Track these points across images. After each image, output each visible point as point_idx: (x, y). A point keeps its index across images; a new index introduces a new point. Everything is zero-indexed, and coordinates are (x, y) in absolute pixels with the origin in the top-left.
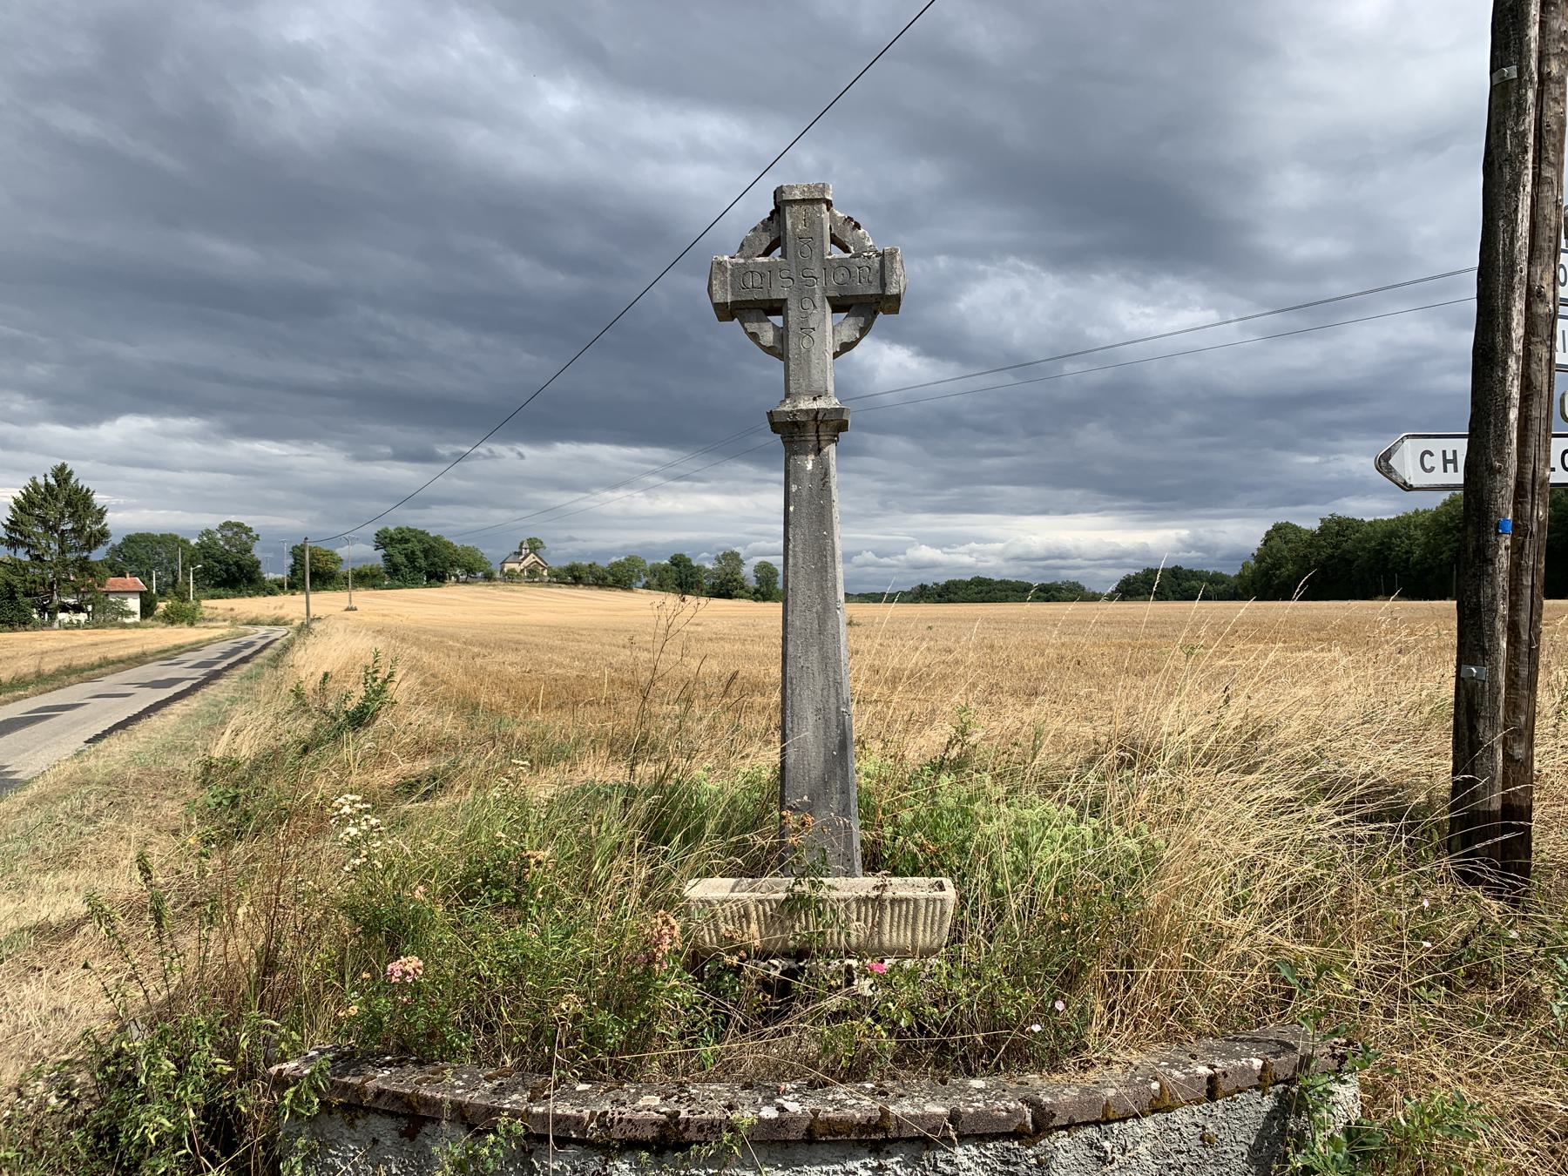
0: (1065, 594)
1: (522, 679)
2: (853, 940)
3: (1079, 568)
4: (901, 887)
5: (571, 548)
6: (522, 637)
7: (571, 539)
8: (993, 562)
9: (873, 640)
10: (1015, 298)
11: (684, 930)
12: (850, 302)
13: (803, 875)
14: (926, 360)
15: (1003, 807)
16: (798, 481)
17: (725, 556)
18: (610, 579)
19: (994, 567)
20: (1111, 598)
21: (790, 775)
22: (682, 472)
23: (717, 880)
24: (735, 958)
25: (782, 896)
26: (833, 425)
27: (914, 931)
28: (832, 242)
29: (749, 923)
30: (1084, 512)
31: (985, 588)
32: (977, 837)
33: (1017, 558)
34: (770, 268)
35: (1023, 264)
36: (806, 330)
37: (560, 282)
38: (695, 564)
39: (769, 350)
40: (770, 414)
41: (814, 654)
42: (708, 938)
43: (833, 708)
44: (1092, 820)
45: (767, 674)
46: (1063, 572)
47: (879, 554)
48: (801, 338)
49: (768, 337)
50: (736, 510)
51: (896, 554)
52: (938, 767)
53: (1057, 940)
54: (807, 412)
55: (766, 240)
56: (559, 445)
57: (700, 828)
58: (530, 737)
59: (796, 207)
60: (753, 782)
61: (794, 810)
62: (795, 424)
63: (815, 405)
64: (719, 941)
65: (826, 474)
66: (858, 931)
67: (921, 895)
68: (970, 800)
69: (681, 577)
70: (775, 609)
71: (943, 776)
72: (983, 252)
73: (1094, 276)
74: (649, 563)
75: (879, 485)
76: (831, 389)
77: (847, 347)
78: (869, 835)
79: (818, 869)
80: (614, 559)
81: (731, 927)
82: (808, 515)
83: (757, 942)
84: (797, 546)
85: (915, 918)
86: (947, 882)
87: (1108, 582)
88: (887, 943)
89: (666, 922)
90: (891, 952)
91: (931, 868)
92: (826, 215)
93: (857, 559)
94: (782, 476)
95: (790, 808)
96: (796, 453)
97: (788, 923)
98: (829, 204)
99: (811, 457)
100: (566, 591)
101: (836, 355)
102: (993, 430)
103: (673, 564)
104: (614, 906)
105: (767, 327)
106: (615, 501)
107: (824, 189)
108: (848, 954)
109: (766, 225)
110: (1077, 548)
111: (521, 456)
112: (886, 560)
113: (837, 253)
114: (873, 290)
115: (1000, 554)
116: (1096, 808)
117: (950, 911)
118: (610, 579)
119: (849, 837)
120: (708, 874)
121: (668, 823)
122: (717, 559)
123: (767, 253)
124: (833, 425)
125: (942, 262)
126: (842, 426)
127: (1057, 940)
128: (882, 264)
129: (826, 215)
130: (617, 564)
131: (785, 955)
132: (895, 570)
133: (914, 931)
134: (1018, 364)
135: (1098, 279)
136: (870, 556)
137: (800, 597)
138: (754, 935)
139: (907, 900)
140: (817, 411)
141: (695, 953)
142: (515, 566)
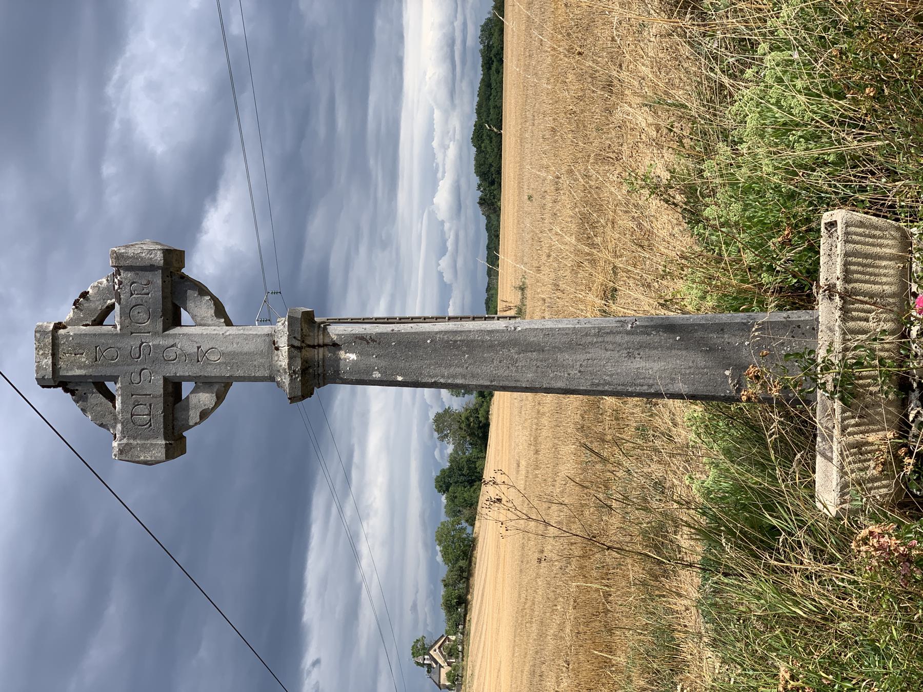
0: (494, 41)
1: (577, 673)
2: (888, 326)
3: (465, 24)
4: (830, 270)
5: (424, 609)
6: (527, 668)
7: (414, 607)
8: (456, 123)
9: (543, 285)
10: (153, 87)
11: (873, 517)
12: (170, 305)
13: (815, 380)
14: (221, 192)
15: (743, 149)
16: (369, 370)
17: (439, 430)
18: (462, 563)
21: (702, 390)
23: (818, 477)
24: (907, 460)
25: (838, 405)
26: (308, 330)
27: (881, 258)
29: (868, 444)
30: (400, 15)
32: (775, 179)
33: (452, 93)
34: (128, 394)
35: (116, 77)
36: (200, 356)
37: (117, 610)
38: (447, 465)
39: (220, 398)
41: (566, 357)
42: (882, 491)
43: (627, 338)
44: (760, 50)
47: (443, 251)
48: (208, 362)
49: (205, 399)
51: (443, 232)
52: (694, 217)
53: (895, 98)
54: (291, 357)
55: (97, 398)
56: (306, 618)
57: (761, 494)
58: (645, 670)
59: (61, 364)
60: (710, 430)
61: (740, 388)
62: (304, 371)
63: (285, 349)
64: (887, 477)
66: (878, 322)
67: (840, 248)
68: (734, 185)
69: (461, 482)
71: (707, 212)
72: (99, 122)
74: (444, 518)
75: (363, 250)
77: (220, 311)
78: (772, 302)
79: (806, 358)
80: (439, 558)
81: (872, 464)
82: (401, 357)
83: (890, 435)
84: (443, 374)
85: (867, 256)
86: (826, 217)
88: (894, 289)
89: (865, 541)
90: (904, 287)
91: (808, 235)
92: (71, 330)
93: (448, 277)
95: (739, 390)
96: (337, 372)
97: (868, 399)
99: (342, 354)
100: (474, 614)
101: (228, 323)
102: (304, 117)
104: (844, 595)
105: (194, 399)
106: (372, 554)
107: (40, 331)
108: (905, 335)
111: (317, 662)
112: (450, 244)
113: (115, 317)
116: (745, 45)
117: (859, 216)
118: (462, 563)
119: (773, 325)
120: (811, 485)
121: (752, 526)
122: (442, 438)
123: (111, 398)
124: (308, 330)
125: (109, 169)
126: (308, 317)
127: (895, 98)
128: (129, 268)
129: (71, 330)
130: (445, 554)
131: (904, 404)
132: (462, 234)
133: (881, 258)
134: (230, 86)
136: (444, 263)
137: (500, 372)
138: (881, 438)
139: (846, 264)
140: (291, 346)
141: (902, 506)
142: (444, 672)
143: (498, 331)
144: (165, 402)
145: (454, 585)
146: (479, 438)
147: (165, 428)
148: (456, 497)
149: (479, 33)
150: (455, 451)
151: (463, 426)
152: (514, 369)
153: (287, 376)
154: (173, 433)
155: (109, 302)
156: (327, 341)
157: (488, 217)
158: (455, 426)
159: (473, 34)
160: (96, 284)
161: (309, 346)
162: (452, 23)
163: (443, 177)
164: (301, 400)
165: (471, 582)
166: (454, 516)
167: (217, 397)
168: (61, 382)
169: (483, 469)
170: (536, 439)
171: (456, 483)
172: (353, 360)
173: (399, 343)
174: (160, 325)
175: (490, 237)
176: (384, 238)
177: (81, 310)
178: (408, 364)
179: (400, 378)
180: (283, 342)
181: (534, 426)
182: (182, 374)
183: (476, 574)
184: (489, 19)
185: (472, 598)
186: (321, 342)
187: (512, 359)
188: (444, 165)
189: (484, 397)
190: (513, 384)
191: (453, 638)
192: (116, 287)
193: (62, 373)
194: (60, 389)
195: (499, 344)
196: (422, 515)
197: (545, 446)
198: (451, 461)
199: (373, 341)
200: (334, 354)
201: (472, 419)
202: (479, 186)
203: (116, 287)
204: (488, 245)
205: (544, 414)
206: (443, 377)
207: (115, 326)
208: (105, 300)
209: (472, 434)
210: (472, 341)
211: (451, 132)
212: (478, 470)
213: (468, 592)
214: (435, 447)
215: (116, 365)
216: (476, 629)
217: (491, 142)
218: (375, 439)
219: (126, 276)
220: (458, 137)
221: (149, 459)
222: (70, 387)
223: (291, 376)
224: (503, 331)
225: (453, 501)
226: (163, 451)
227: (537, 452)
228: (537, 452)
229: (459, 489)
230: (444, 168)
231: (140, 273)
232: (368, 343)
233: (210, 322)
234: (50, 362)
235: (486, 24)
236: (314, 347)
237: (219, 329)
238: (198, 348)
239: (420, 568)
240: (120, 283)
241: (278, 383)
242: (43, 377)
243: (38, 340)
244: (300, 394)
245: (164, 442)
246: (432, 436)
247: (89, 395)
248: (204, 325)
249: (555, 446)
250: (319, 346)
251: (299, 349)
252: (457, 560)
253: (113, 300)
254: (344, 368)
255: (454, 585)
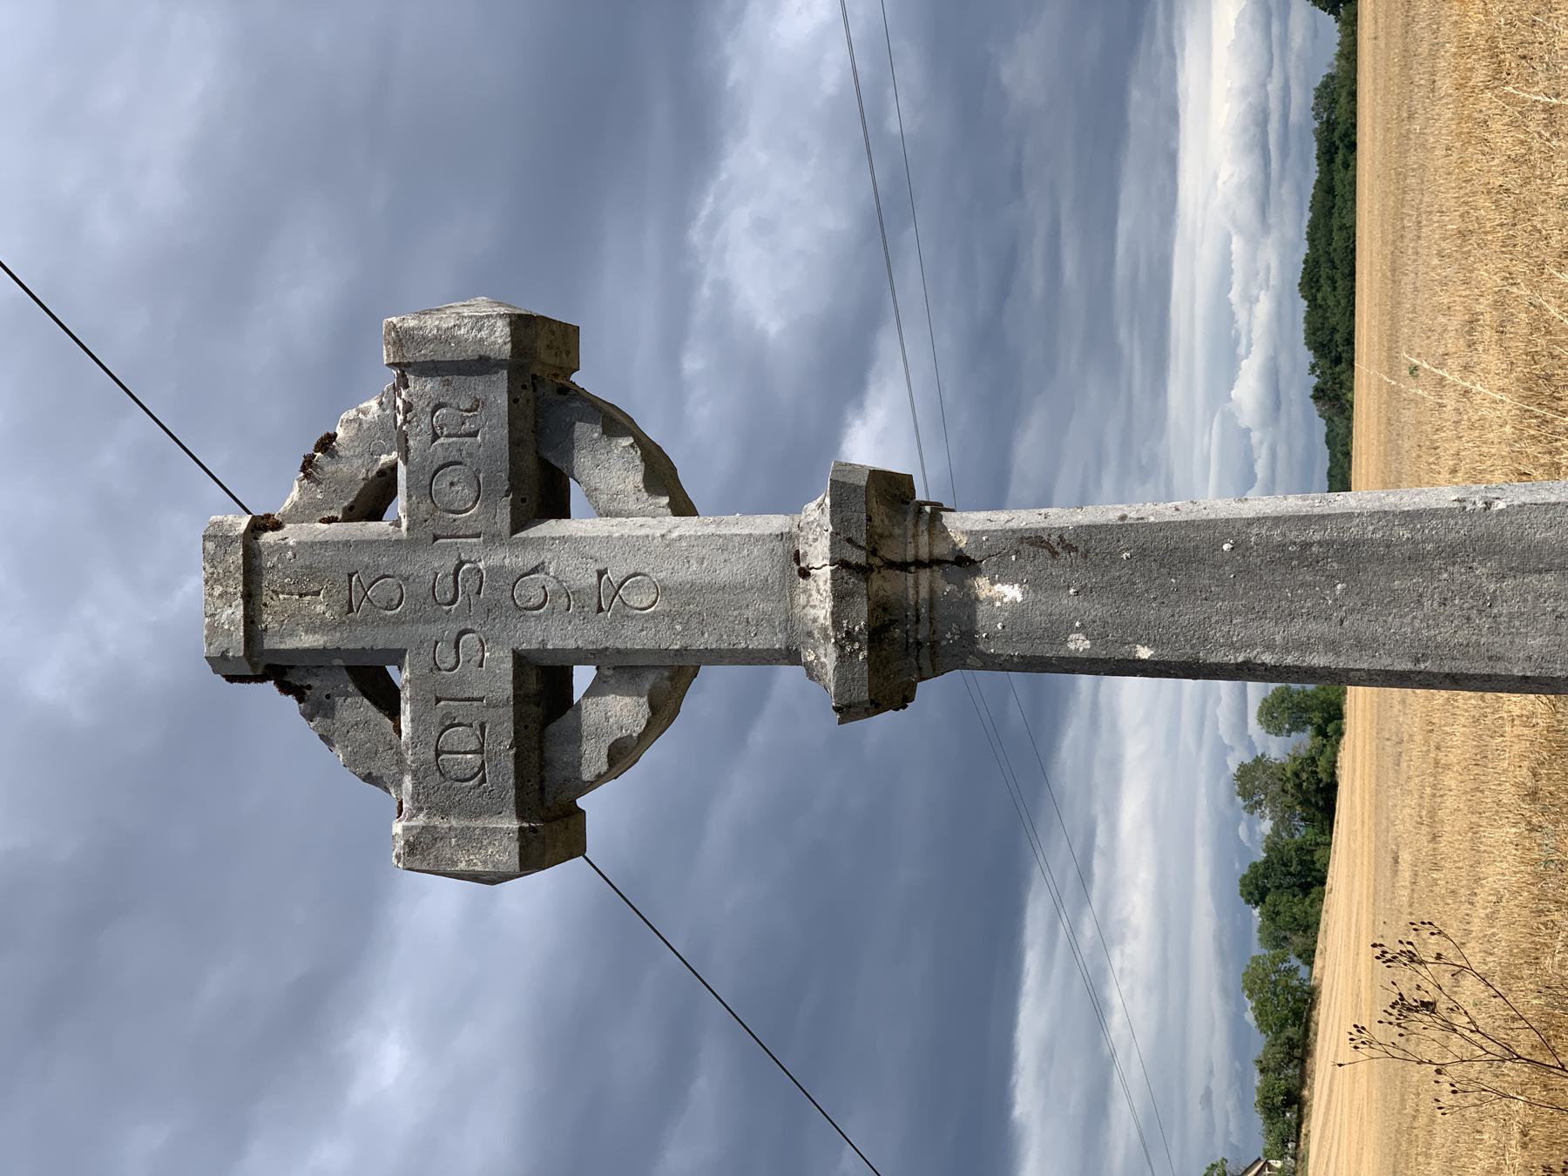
0: (1340, 113)
5: (1225, 1102)
7: (1207, 1098)
8: (1270, 256)
10: (764, 227)
12: (530, 464)
14: (872, 392)
17: (1245, 793)
18: (1291, 1031)
19: (1281, 253)
20: (1350, 26)
22: (1072, 873)
28: (377, 516)
31: (1324, 271)
33: (1263, 206)
35: (704, 213)
36: (605, 596)
38: (1262, 855)
39: (662, 712)
40: (847, 711)
45: (1527, 720)
46: (1295, 116)
48: (625, 613)
49: (621, 712)
50: (1154, 767)
54: (840, 596)
55: (357, 709)
59: (267, 618)
62: (877, 634)
63: (823, 575)
65: (1035, 541)
70: (1359, 702)
72: (679, 286)
73: (730, 83)
74: (1257, 949)
76: (777, 523)
77: (660, 476)
80: (1250, 1017)
82: (1160, 597)
87: (1315, 33)
92: (292, 534)
94: (1085, 681)
96: (969, 635)
98: (261, 524)
99: (983, 587)
100: (1315, 1124)
101: (682, 507)
103: (1260, 901)
107: (217, 538)
109: (317, 708)
110: (1245, 92)
112: (1261, 469)
114: (497, 393)
115: (1253, 243)
118: (1291, 1031)
122: (1253, 807)
125: (693, 364)
128: (429, 369)
129: (292, 534)
130: (1261, 1014)
132: (1281, 451)
134: (882, 223)
135: (736, 74)
137: (1444, 633)
140: (841, 565)
143: (1433, 513)
144: (519, 720)
145: (1278, 1070)
146: (1318, 809)
147: (520, 787)
148: (1278, 914)
149: (1312, 102)
150: (1276, 831)
151: (1289, 786)
152: (1487, 624)
153: (831, 648)
154: (542, 800)
155: (384, 459)
156: (941, 550)
157: (1329, 421)
158: (1275, 788)
159: (1302, 102)
160: (352, 413)
161: (891, 565)
162: (1264, 85)
163: (1249, 352)
164: (868, 713)
165: (1308, 1066)
166: (1276, 947)
167: (654, 708)
168: (268, 667)
169: (1326, 865)
170: (1432, 814)
171: (1277, 888)
172: (1013, 602)
173: (1142, 553)
174: (503, 516)
175: (1333, 457)
176: (1144, 460)
177: (318, 483)
178: (1166, 612)
179: (1144, 653)
180: (819, 554)
181: (1428, 790)
182: (560, 644)
183: (1318, 1053)
184: (1331, 77)
185: (1312, 1094)
186: (924, 554)
187: (1479, 593)
188: (1250, 332)
189: (1325, 736)
190: (1483, 668)
191: (1278, 1164)
192: (400, 418)
193: (271, 643)
194: (270, 685)
195: (1438, 553)
196: (1218, 937)
197: (1453, 829)
198: (1269, 849)
199: (1069, 548)
200: (961, 586)
201: (1304, 776)
202: (1313, 367)
203: (400, 418)
204: (1330, 469)
205: (1448, 767)
206: (1270, 647)
207: (397, 523)
208: (374, 455)
209: (1305, 803)
210: (1356, 544)
211: (1262, 273)
212: (1318, 866)
213: (1303, 1084)
214: (1239, 820)
215: (398, 621)
216: (1319, 1150)
217: (1335, 289)
218: (1133, 806)
219: (423, 388)
220: (1274, 281)
221: (479, 868)
222: (293, 679)
223: (840, 646)
224: (1450, 513)
225: (1273, 920)
226: (514, 847)
227: (1434, 838)
228: (1434, 838)
229: (1285, 898)
230: (1249, 339)
231: (457, 380)
232: (1054, 554)
233: (632, 506)
234: (240, 613)
235: (1325, 85)
236: (903, 566)
237: (662, 524)
238: (601, 574)
239: (1215, 1036)
240: (408, 407)
241: (809, 669)
242: (224, 655)
243: (211, 559)
244: (865, 696)
245: (515, 825)
246: (1232, 801)
247: (339, 701)
248: (618, 514)
249: (1474, 828)
250: (919, 564)
251: (864, 571)
252: (1283, 1026)
253: (394, 455)
254: (988, 623)
255: (1278, 1070)
